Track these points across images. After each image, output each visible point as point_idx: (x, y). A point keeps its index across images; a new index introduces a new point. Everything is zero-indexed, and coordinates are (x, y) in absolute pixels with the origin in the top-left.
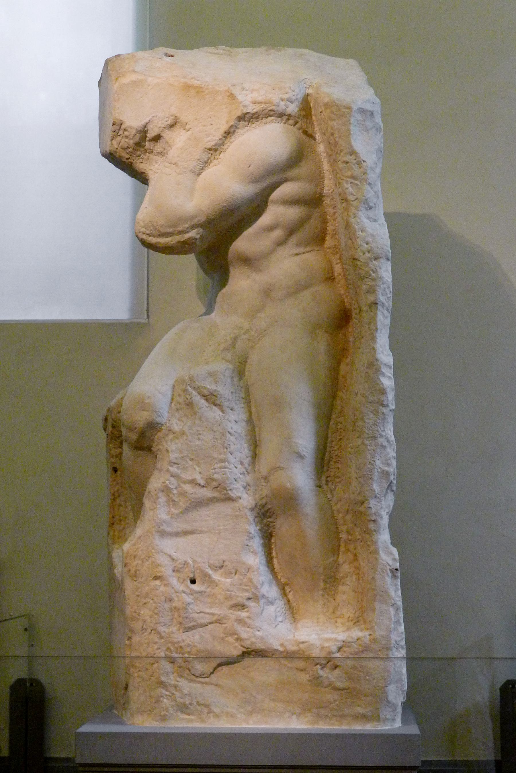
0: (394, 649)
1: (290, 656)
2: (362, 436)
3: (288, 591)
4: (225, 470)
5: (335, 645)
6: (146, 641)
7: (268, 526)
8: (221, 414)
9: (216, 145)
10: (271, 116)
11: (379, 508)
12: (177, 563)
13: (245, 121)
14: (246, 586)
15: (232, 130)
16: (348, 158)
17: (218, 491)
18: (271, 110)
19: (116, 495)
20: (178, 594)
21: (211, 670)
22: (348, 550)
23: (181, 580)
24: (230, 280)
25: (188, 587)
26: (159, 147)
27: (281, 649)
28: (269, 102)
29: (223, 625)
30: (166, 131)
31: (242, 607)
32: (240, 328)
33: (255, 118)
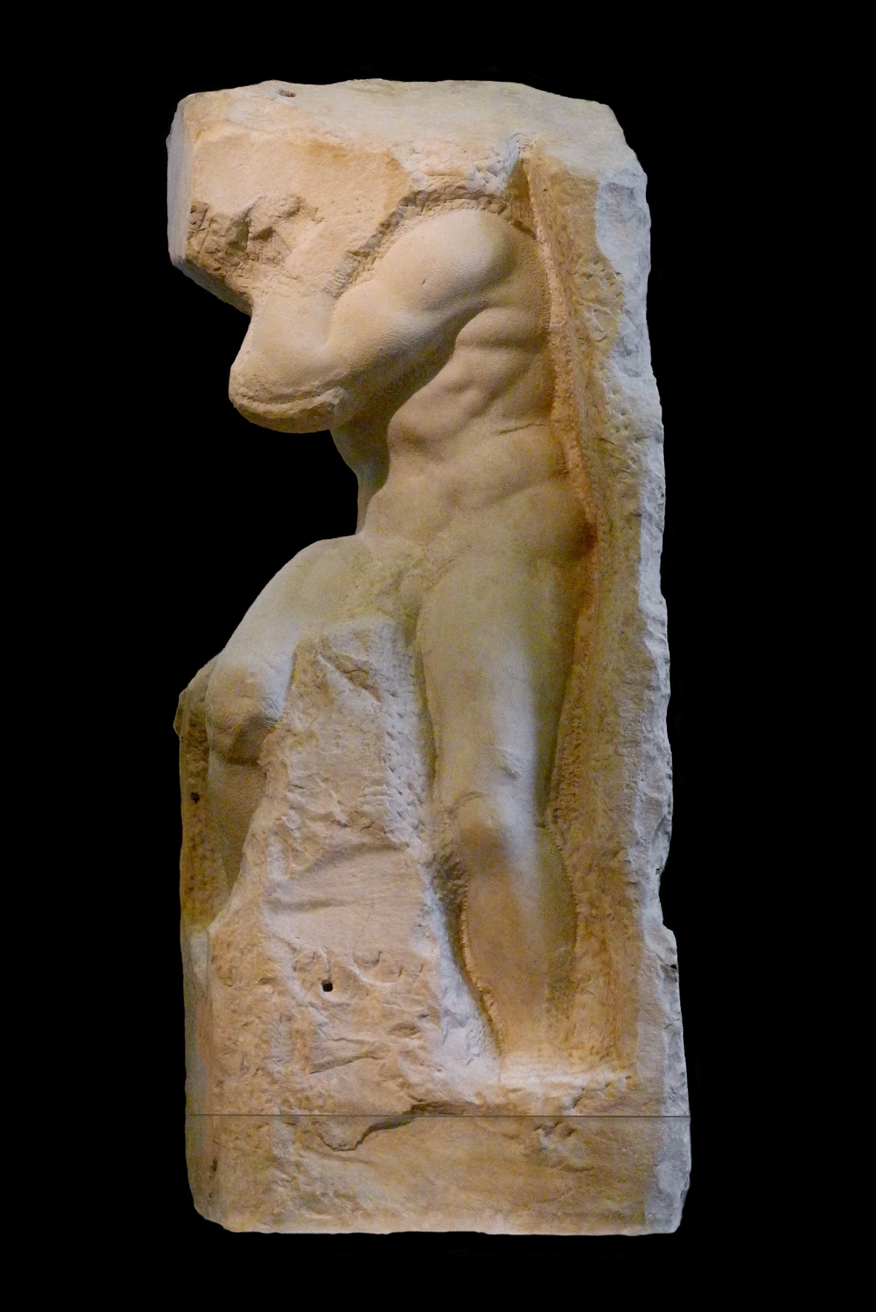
0: (669, 1102)
1: (492, 1113)
2: (615, 740)
3: (488, 1004)
4: (382, 797)
5: (569, 1094)
6: (249, 1088)
7: (455, 892)
8: (376, 702)
9: (367, 246)
10: (460, 197)
11: (643, 862)
12: (301, 955)
13: (416, 205)
14: (418, 994)
15: (394, 221)
16: (591, 268)
17: (371, 834)
18: (460, 187)
19: (198, 840)
20: (302, 1008)
21: (359, 1138)
22: (591, 934)
23: (308, 985)
24: (391, 475)
25: (318, 996)
26: (269, 249)
27: (477, 1101)
28: (456, 174)
29: (379, 1061)
30: (282, 222)
31: (411, 1029)
32: (408, 556)
33: (433, 201)
